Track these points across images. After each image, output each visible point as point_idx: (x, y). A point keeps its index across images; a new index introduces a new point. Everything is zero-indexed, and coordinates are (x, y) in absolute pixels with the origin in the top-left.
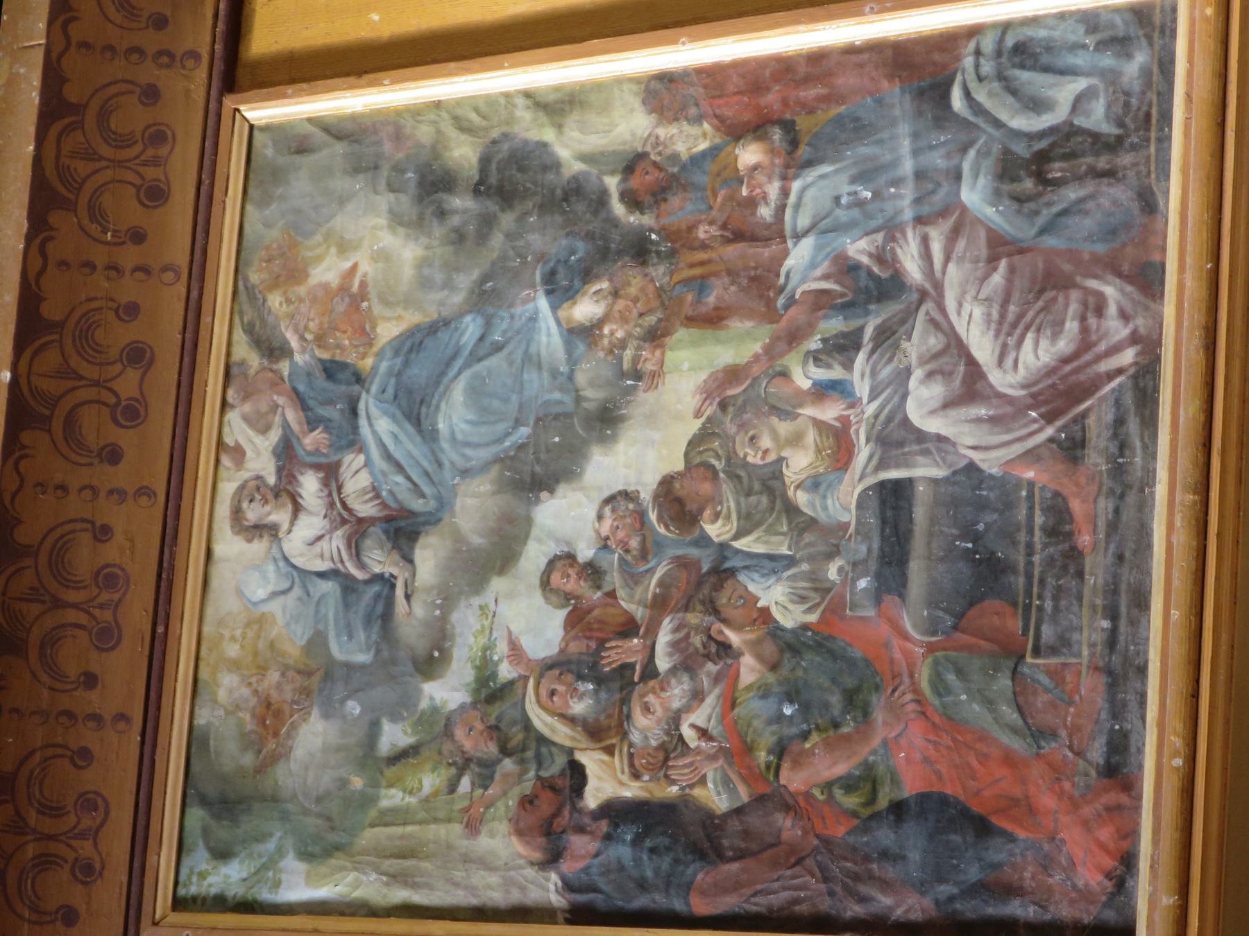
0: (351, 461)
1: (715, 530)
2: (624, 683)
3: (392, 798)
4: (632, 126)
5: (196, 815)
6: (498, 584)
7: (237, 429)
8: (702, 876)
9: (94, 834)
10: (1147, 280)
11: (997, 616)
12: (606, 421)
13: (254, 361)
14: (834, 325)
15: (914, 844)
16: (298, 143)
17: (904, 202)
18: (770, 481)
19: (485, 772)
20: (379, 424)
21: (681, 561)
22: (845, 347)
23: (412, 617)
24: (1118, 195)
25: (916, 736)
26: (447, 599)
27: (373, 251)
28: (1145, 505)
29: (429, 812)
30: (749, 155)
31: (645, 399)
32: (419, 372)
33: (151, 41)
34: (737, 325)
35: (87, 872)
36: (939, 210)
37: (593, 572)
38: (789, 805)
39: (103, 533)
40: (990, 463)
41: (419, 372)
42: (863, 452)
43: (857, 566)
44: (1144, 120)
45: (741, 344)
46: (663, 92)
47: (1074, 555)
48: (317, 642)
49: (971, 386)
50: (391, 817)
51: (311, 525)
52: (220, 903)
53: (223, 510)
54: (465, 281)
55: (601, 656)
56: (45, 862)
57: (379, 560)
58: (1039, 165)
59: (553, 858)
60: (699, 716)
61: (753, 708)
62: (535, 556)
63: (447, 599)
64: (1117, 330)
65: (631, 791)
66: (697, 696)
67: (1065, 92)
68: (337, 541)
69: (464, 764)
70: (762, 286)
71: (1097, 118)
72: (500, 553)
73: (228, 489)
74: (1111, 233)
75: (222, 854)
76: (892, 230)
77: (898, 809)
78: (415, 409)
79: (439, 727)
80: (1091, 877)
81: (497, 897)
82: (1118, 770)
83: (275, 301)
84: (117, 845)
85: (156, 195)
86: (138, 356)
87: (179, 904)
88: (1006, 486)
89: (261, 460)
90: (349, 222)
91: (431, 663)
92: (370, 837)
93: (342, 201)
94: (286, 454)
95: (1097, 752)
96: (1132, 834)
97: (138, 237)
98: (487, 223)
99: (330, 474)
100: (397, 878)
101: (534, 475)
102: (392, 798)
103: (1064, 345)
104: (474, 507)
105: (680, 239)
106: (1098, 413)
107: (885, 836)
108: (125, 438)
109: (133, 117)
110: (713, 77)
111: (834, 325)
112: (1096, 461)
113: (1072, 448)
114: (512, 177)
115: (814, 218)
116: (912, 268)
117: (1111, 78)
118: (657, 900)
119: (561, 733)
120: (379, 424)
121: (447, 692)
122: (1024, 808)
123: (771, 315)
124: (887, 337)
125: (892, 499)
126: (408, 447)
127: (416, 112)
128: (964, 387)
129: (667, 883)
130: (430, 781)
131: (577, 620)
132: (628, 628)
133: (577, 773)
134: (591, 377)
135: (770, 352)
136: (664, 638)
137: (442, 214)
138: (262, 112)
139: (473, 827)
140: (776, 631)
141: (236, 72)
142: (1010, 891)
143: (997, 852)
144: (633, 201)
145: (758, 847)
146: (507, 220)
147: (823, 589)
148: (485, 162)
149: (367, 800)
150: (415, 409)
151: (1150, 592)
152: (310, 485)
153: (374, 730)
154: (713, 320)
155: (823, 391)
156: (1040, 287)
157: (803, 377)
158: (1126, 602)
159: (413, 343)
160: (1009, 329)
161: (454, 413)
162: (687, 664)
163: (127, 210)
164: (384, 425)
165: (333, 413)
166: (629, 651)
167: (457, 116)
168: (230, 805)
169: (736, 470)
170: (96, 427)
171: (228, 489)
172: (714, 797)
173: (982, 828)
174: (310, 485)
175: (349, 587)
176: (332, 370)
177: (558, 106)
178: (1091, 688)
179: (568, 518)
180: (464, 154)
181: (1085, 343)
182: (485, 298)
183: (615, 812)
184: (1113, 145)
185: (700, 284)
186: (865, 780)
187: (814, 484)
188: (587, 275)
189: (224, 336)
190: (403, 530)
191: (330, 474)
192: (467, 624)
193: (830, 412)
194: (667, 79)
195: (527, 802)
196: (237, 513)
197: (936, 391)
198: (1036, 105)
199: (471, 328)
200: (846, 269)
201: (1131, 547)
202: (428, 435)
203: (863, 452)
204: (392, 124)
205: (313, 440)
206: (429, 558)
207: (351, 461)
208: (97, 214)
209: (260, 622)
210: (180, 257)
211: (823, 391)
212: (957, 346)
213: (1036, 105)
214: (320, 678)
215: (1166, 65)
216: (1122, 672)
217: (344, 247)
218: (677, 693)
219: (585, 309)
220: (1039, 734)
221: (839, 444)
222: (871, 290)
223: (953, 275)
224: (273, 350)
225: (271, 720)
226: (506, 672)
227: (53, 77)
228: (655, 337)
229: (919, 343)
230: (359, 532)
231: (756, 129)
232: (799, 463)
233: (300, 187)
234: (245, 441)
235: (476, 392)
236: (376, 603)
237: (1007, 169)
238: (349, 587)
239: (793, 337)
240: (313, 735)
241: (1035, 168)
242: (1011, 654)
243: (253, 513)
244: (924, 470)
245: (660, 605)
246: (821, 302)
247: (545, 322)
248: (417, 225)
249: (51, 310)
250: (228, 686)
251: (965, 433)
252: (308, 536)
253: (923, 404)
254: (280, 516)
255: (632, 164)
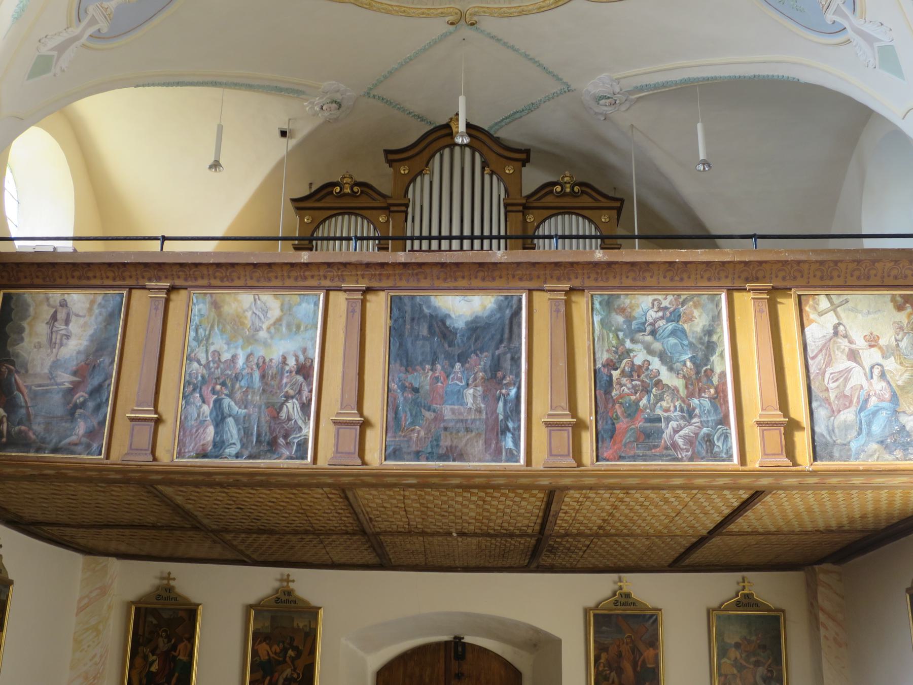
0: (664, 322)
1: (654, 390)
2: (630, 376)
3: (611, 335)
4: (718, 370)
5: (606, 297)
6: (645, 352)
7: (670, 298)
8: (602, 392)
9: (602, 280)
10: (691, 459)
11: (642, 437)
12: (671, 369)
13: (681, 300)
14: (685, 408)
15: (609, 427)
16: (718, 305)
17: (704, 419)
18: (662, 399)
19: (616, 352)
20: (671, 326)
21: (650, 384)
22: (682, 410)
23: (639, 336)
24: (704, 453)
25: (625, 426)
26: (642, 343)
27: (698, 322)
28: (658, 460)
29: (609, 343)
30: (712, 391)
31: (674, 375)
32: (679, 333)
33: (736, 276)
34: (685, 391)
35: (596, 280)
36: (703, 424)
37: (647, 369)
38: (613, 406)
39: (652, 277)
40: (664, 435)
41: (679, 333)
42: (666, 414)
43: (649, 415)
44: (715, 457)
45: (683, 392)
46: (723, 375)
47: (651, 449)
48: (635, 318)
49: (676, 431)
50: (608, 335)
51: (654, 315)
52: (593, 304)
53: (656, 297)
54: (694, 341)
55: (636, 371)
56: (597, 273)
57: (648, 329)
58: (709, 440)
59: (604, 366)
60: (626, 390)
61: (627, 398)
62: (650, 358)
63: (642, 343)
64: (684, 454)
65: (614, 379)
66: (629, 389)
67: (720, 444)
68: (651, 321)
69: (617, 348)
70: (691, 395)
71: (716, 449)
72: (650, 352)
73: (660, 297)
74: (698, 452)
75: (600, 303)
76: (700, 417)
77: (613, 424)
78: (673, 333)
79: (621, 342)
80: (605, 455)
81: (597, 356)
82: (621, 458)
83: (691, 303)
84: (601, 284)
85: (709, 279)
86: (682, 279)
87: (592, 296)
88: (661, 438)
89: (665, 303)
90: (704, 316)
91: (633, 341)
92: (605, 332)
93: (708, 315)
94: (666, 308)
95: (623, 455)
96: (611, 460)
97: (702, 277)
98: (702, 344)
99: (662, 318)
100: (599, 339)
101: (663, 357)
102: (611, 335)
103: (682, 446)
104: (657, 346)
105: (699, 380)
106: (672, 452)
107: (610, 422)
108: (668, 279)
109: (723, 274)
110: (725, 384)
111: (685, 408)
112: (665, 452)
113: (667, 448)
114: (711, 347)
115: (700, 403)
116: (694, 421)
117: (722, 451)
118: (598, 385)
119: (622, 366)
120: (671, 326)
121: (628, 344)
122: (614, 444)
123: (687, 397)
124: (683, 418)
125: (659, 420)
126: (667, 332)
127: (722, 328)
128: (678, 431)
129: (601, 386)
130: (614, 342)
131: (640, 367)
132: (639, 376)
133: (616, 369)
134: (678, 365)
135: (681, 397)
136: (637, 383)
137: (705, 335)
138: (723, 296)
139: (607, 351)
140: (639, 401)
141: (730, 291)
142: (603, 442)
143: (608, 440)
144: (706, 371)
145: (607, 400)
146: (703, 348)
147: (645, 409)
148: (713, 342)
149: (610, 330)
150: (673, 333)
151: (537, 631)
152: (660, 314)
153: (621, 331)
154: (686, 387)
155: (675, 407)
156: (690, 441)
157: (677, 404)
158: (644, 458)
159: (683, 331)
160: (684, 437)
161: (672, 341)
162: (634, 387)
163: (706, 275)
164: (670, 327)
165: (672, 318)
166: (635, 375)
167: (721, 337)
168: (608, 304)
169: (663, 393)
170: (669, 274)
171: (660, 297)
172: (614, 393)
173: (612, 437)
174: (660, 314)
175: (644, 324)
176: (679, 316)
177: (722, 355)
178: (632, 453)
179: (656, 364)
180: (715, 338)
181: (682, 449)
182: (691, 345)
183: (611, 376)
184: (711, 453)
185: (692, 384)
186: (617, 418)
187: (661, 407)
188: (694, 363)
189: (685, 294)
190: (653, 333)
191: (662, 318)
192: (639, 347)
193: (672, 409)
194: (725, 375)
195: (612, 361)
196: (655, 300)
197: (675, 426)
198: (718, 440)
199: (686, 342)
200: (694, 409)
201: (653, 458)
202: (668, 337)
203: (666, 414)
204: (720, 324)
205: (668, 314)
206: (649, 338)
207: (664, 322)
208: (705, 271)
209: (638, 306)
210: (699, 285)
211: (675, 407)
212: (682, 429)
213: (718, 440)
214: (629, 319)
215: (723, 460)
216: (634, 458)
217: (700, 316)
218: (629, 386)
219: (689, 364)
220: (625, 445)
221: (667, 410)
222: (690, 414)
223: (692, 427)
224: (683, 304)
225: (622, 311)
226: (631, 355)
227: (729, 262)
228: (684, 377)
229: (682, 423)
230: (653, 324)
231: (717, 392)
232: (664, 404)
233: (711, 306)
234: (667, 300)
235: (675, 344)
236: (641, 330)
237: (708, 435)
238: (644, 324)
239: (684, 401)
240: (620, 319)
241: (709, 440)
242: (637, 440)
243: (656, 303)
244: (663, 425)
245: (642, 381)
246: (689, 405)
247: (686, 357)
248: (703, 331)
249: (689, 265)
250: (627, 301)
251: (668, 432)
252: (652, 315)
253: (673, 424)
254: (655, 309)
255: (712, 370)
